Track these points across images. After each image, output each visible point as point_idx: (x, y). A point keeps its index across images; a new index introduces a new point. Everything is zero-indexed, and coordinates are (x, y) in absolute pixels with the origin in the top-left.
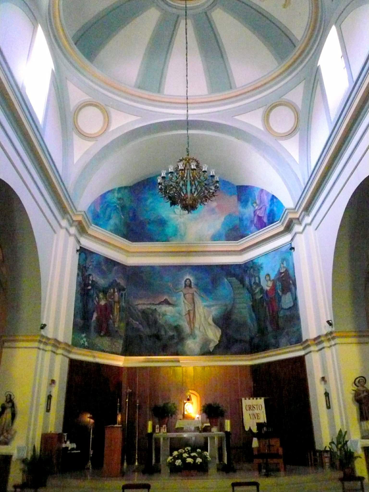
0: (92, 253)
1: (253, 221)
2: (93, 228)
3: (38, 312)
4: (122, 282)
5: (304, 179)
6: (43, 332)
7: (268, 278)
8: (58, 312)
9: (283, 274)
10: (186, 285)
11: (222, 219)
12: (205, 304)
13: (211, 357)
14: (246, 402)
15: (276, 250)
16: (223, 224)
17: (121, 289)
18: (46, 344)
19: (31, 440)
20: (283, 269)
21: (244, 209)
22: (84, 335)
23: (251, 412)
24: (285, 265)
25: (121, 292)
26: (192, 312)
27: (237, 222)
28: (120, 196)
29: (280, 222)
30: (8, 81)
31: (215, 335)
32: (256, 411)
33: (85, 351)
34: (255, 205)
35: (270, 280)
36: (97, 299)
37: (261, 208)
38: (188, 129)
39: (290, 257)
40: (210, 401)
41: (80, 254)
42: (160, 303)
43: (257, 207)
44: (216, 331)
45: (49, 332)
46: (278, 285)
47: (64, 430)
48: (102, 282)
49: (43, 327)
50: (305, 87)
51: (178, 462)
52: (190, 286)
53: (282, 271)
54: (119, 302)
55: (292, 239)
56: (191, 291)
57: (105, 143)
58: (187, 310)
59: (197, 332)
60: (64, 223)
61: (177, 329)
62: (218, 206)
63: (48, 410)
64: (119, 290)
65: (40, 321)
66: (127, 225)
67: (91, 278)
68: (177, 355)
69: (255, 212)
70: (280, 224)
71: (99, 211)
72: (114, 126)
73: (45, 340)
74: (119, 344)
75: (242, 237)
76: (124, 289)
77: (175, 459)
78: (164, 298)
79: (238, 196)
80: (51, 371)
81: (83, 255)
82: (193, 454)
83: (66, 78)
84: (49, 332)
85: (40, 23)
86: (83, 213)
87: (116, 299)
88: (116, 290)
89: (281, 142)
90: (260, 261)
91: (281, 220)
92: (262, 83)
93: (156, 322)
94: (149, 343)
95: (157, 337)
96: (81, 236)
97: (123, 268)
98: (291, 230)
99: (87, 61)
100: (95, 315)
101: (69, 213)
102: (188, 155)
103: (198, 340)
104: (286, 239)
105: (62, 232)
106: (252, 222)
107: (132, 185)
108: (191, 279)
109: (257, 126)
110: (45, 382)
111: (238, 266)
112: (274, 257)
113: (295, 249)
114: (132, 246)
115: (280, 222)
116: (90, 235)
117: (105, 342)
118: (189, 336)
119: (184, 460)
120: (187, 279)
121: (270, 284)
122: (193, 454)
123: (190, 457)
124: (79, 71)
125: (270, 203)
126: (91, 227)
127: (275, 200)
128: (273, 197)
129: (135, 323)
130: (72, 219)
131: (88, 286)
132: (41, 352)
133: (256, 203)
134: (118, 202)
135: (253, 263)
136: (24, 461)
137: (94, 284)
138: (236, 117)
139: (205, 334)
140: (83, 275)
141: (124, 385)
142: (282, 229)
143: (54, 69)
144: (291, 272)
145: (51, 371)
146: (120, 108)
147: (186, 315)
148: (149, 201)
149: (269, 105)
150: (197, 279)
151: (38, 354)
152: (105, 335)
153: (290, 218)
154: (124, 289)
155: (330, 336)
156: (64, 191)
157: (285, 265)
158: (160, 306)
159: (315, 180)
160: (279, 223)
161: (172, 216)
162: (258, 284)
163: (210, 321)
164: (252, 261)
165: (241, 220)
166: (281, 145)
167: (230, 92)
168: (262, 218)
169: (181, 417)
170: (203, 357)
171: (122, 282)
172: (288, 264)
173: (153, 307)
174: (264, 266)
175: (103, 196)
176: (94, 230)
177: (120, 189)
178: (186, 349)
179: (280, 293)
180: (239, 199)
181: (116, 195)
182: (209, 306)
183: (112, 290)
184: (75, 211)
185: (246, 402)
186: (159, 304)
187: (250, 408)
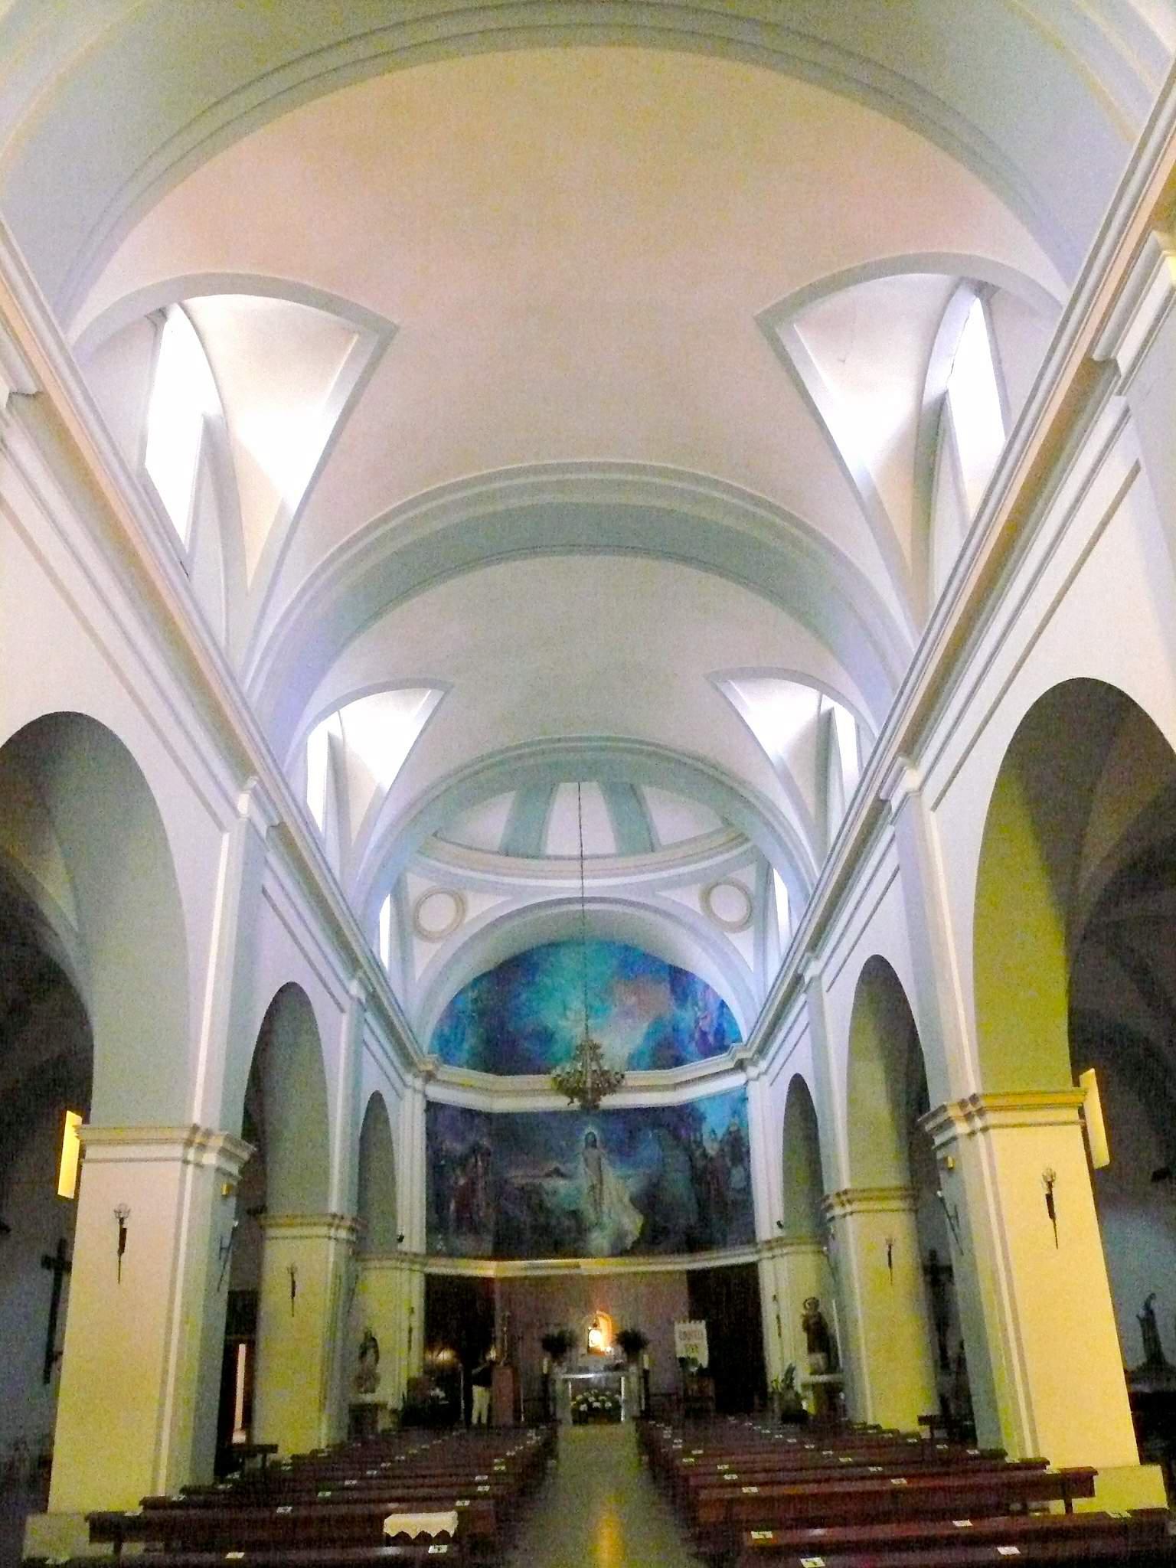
11: (644, 1027)
12: (619, 1173)
13: (627, 1260)
14: (680, 1327)
16: (648, 1036)
22: (440, 1236)
23: (686, 1342)
31: (634, 1222)
32: (694, 1341)
33: (443, 1261)
35: (716, 1139)
38: (583, 911)
40: (628, 1326)
42: (548, 1175)
45: (404, 1246)
49: (401, 1239)
51: (584, 1407)
56: (595, 1152)
59: (605, 1219)
61: (575, 1214)
62: (640, 1002)
63: (410, 1348)
65: (395, 1231)
66: (489, 1042)
68: (576, 1256)
69: (697, 1022)
72: (472, 913)
74: (488, 1246)
77: (580, 1403)
78: (553, 1167)
82: (601, 1398)
87: (480, 1171)
93: (541, 1205)
95: (544, 1230)
97: (489, 1117)
102: (580, 1419)
103: (607, 1232)
104: (736, 1080)
105: (408, 1093)
106: (692, 1037)
108: (596, 1133)
110: (405, 1310)
111: (671, 1109)
116: (438, 1081)
117: (466, 1242)
119: (590, 1405)
120: (590, 1133)
121: (716, 1146)
122: (601, 1398)
123: (597, 1401)
133: (697, 1005)
141: (498, 1305)
142: (732, 1065)
146: (482, 889)
148: (524, 997)
150: (603, 1130)
151: (184, 1174)
155: (779, 1242)
161: (563, 1023)
162: (699, 1144)
163: (626, 1199)
165: (675, 1029)
166: (730, 943)
169: (585, 1351)
170: (619, 1260)
173: (537, 1181)
175: (453, 1002)
176: (447, 1072)
179: (729, 1164)
180: (673, 991)
182: (626, 1178)
183: (473, 1160)
185: (680, 1327)
187: (686, 1335)
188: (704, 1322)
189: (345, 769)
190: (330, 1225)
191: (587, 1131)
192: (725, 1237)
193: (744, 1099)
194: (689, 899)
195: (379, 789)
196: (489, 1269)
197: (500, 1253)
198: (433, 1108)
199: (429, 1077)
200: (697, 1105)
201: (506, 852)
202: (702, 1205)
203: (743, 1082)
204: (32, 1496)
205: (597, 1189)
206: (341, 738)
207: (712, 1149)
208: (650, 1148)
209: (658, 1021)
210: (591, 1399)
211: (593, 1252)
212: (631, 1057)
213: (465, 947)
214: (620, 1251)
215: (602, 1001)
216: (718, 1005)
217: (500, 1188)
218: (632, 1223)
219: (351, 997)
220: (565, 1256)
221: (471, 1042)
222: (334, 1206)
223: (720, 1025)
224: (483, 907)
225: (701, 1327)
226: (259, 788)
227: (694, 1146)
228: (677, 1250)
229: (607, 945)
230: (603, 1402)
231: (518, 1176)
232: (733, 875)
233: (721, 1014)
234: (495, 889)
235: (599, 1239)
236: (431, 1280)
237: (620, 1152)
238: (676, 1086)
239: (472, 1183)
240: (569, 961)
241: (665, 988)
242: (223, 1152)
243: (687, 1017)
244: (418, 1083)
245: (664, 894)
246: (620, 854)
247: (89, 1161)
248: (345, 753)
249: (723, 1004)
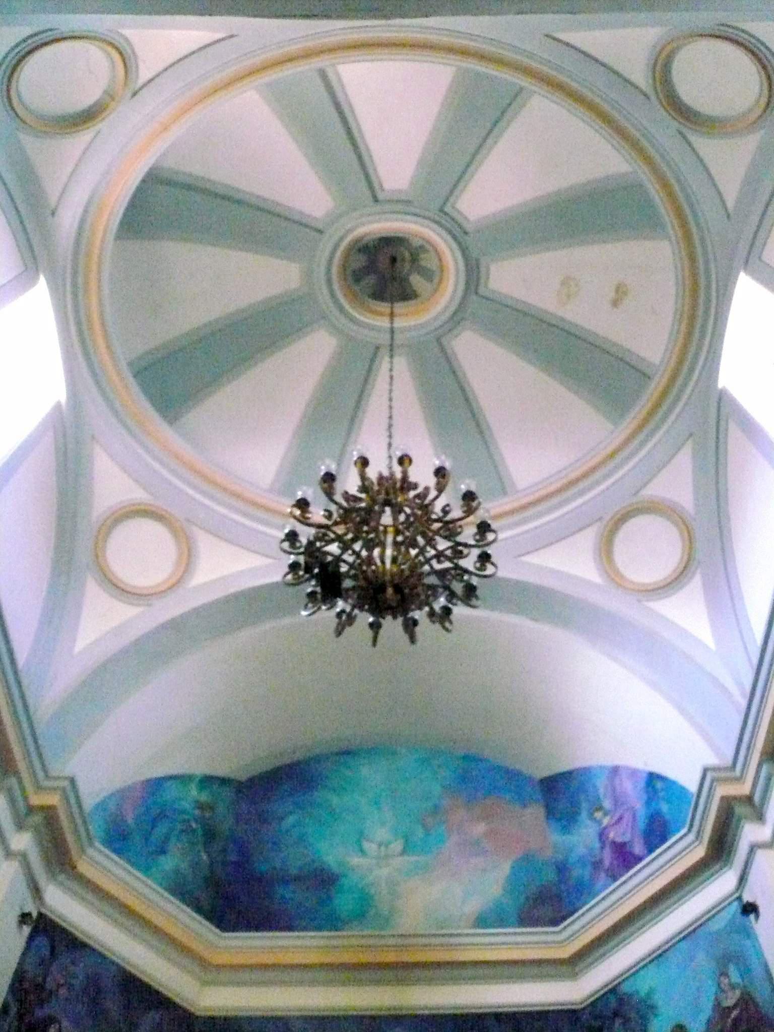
1: (601, 861)
2: (99, 858)
5: (740, 685)
9: (735, 1013)
11: (506, 868)
15: (689, 934)
16: (513, 881)
20: (730, 994)
21: (569, 837)
24: (735, 976)
27: (550, 875)
28: (204, 797)
29: (689, 830)
30: (18, 724)
34: (598, 815)
37: (620, 819)
39: (748, 943)
41: (31, 938)
43: (606, 821)
50: (694, 457)
53: (729, 1002)
55: (742, 880)
62: (491, 834)
66: (212, 882)
69: (602, 835)
70: (691, 837)
71: (130, 821)
79: (547, 806)
81: (42, 942)
83: (93, 437)
85: (44, 272)
86: (66, 783)
90: (642, 985)
91: (691, 826)
92: (585, 468)
96: (52, 876)
98: (730, 852)
99: (152, 413)
101: (17, 773)
107: (243, 776)
109: (580, 574)
112: (692, 959)
113: (761, 910)
114: (222, 943)
115: (689, 830)
124: (134, 436)
125: (645, 797)
126: (90, 851)
127: (659, 785)
128: (653, 778)
130: (26, 798)
133: (600, 808)
134: (197, 812)
135: (621, 1001)
138: (524, 559)
142: (699, 852)
148: (291, 820)
149: (607, 518)
153: (723, 798)
156: (29, 740)
157: (735, 976)
159: (761, 729)
160: (685, 835)
161: (356, 860)
164: (613, 991)
165: (562, 869)
166: (662, 617)
167: (506, 500)
168: (628, 849)
172: (746, 971)
174: (659, 999)
175: (156, 785)
177: (207, 781)
180: (551, 813)
181: (194, 792)
184: (41, 775)
200: (626, 988)
209: (527, 861)
215: (427, 831)
226: (69, 788)
232: (650, 491)
241: (535, 813)
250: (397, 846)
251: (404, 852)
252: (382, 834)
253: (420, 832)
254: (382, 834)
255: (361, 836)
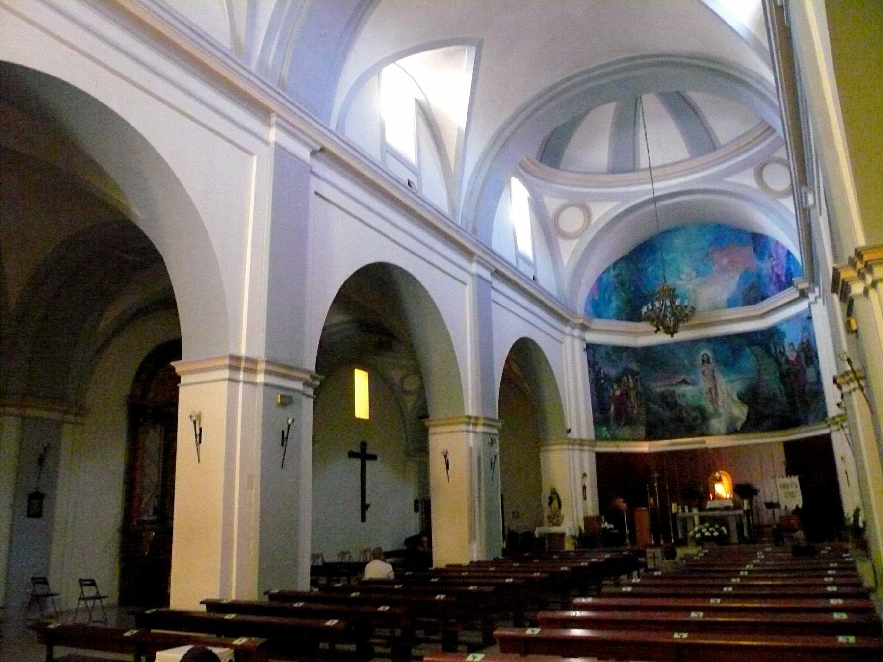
0: (600, 346)
3: (562, 420)
4: (634, 366)
6: (569, 436)
7: (792, 348)
8: (578, 417)
10: (704, 361)
11: (738, 276)
16: (739, 284)
17: (634, 374)
18: (573, 444)
19: (576, 522)
22: (605, 428)
23: (787, 490)
25: (636, 376)
26: (713, 391)
27: (754, 279)
35: (794, 349)
36: (612, 391)
43: (774, 263)
44: (743, 408)
45: (574, 435)
46: (801, 356)
47: (601, 513)
48: (613, 372)
49: (569, 431)
52: (709, 362)
54: (634, 388)
56: (711, 366)
57: (590, 238)
58: (708, 387)
59: (721, 411)
60: (567, 330)
61: (701, 410)
63: (585, 498)
64: (633, 376)
67: (602, 371)
69: (772, 267)
72: (595, 218)
73: (573, 442)
74: (642, 431)
75: (763, 298)
76: (638, 374)
77: (695, 533)
80: (582, 467)
82: (711, 529)
84: (574, 435)
87: (631, 386)
88: (630, 377)
89: (779, 200)
90: (784, 328)
94: (672, 426)
95: (679, 419)
99: (552, 170)
100: (612, 408)
103: (723, 418)
104: (802, 306)
105: (568, 340)
106: (771, 279)
110: (579, 475)
117: (627, 431)
118: (713, 416)
119: (703, 534)
121: (795, 354)
129: (655, 407)
131: (600, 381)
132: (571, 452)
133: (772, 256)
136: (574, 537)
137: (607, 378)
139: (731, 413)
140: (594, 370)
143: (583, 528)
144: (812, 342)
145: (582, 467)
147: (707, 393)
148: (650, 269)
150: (714, 352)
152: (626, 424)
154: (638, 374)
158: (679, 386)
161: (679, 283)
162: (783, 354)
165: (759, 276)
171: (634, 366)
173: (672, 389)
174: (787, 333)
175: (600, 280)
176: (598, 323)
178: (711, 430)
182: (732, 382)
183: (625, 378)
186: (676, 385)
188: (797, 477)
189: (435, 121)
190: (468, 424)
191: (702, 353)
192: (806, 417)
193: (810, 318)
194: (747, 180)
195: (459, 130)
196: (644, 447)
197: (650, 436)
198: (591, 348)
199: (584, 328)
201: (613, 171)
202: (790, 395)
203: (807, 306)
204: (796, 543)
205: (713, 393)
206: (425, 100)
207: (792, 356)
208: (749, 360)
210: (704, 530)
211: (714, 432)
212: (729, 300)
213: (595, 240)
214: (732, 431)
216: (786, 253)
217: (646, 396)
218: (740, 412)
219: (472, 275)
220: (693, 437)
221: (615, 303)
222: (471, 409)
223: (789, 269)
224: (602, 212)
225: (795, 479)
226: (279, 120)
227: (780, 356)
228: (772, 429)
229: (703, 226)
230: (712, 532)
231: (659, 387)
233: (788, 260)
234: (608, 198)
235: (716, 424)
236: (599, 456)
237: (726, 364)
238: (763, 316)
239: (625, 394)
240: (678, 241)
241: (749, 250)
242: (268, 372)
243: (766, 266)
244: (577, 332)
245: (729, 179)
246: (691, 159)
247: (184, 385)
248: (431, 109)
249: (789, 253)
250: (694, 274)
251: (696, 276)
252: (687, 269)
253: (702, 267)
254: (687, 269)
255: (679, 271)
